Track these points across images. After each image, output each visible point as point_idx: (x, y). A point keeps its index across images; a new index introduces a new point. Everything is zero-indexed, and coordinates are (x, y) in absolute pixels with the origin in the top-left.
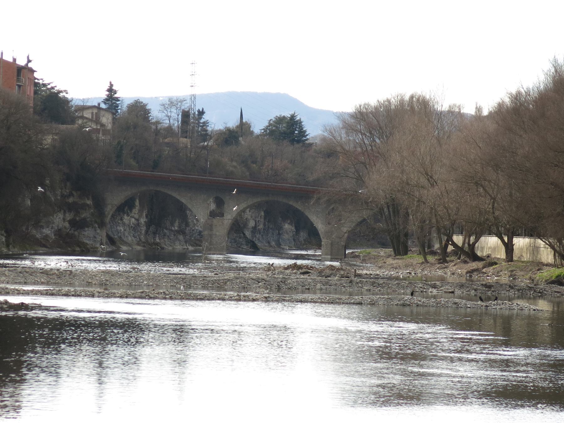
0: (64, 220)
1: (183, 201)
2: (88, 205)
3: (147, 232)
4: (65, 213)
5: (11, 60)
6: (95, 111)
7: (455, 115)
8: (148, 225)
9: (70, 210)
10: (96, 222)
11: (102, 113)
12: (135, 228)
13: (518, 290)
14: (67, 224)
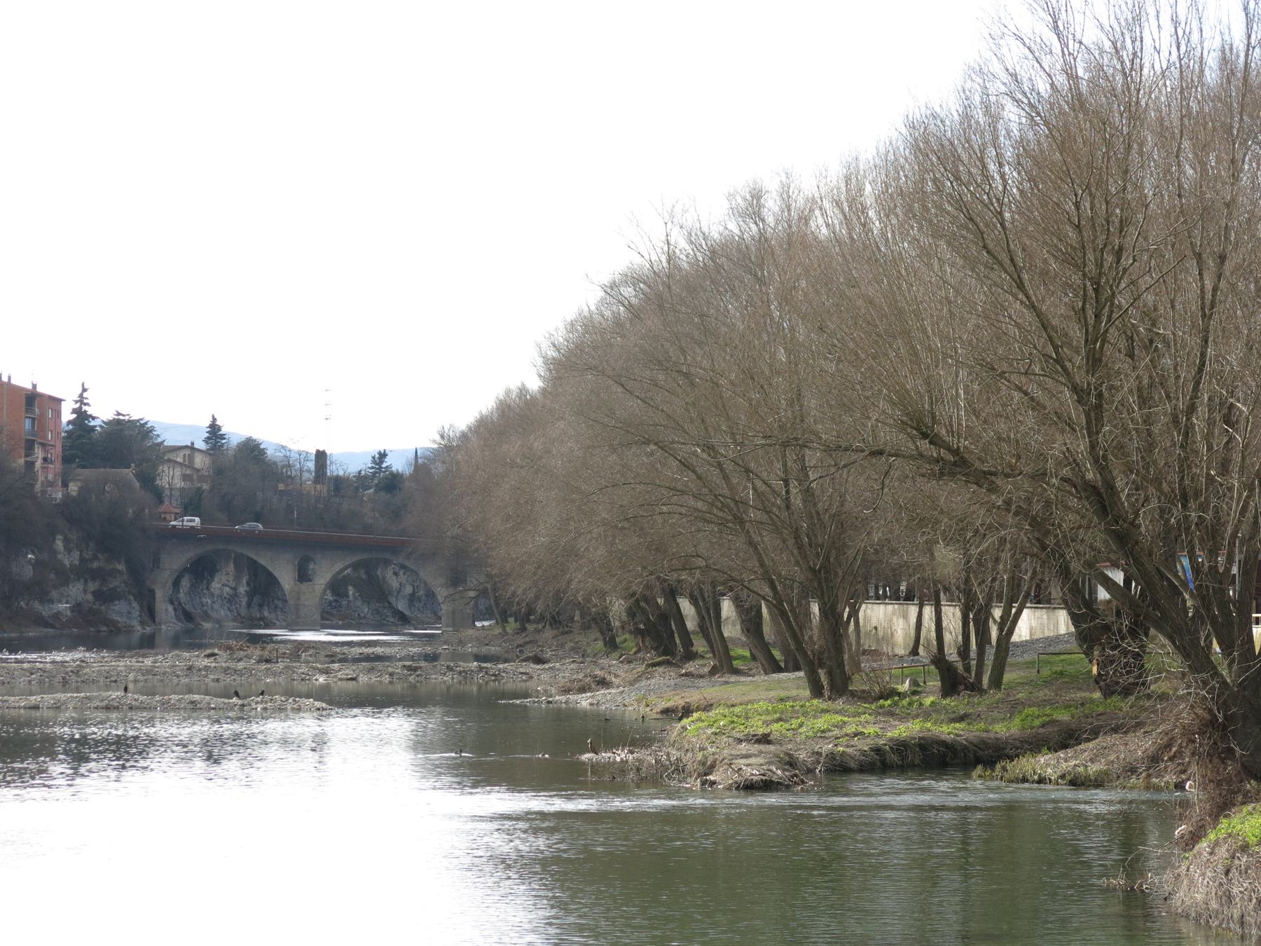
0: (85, 591)
1: (262, 562)
2: (119, 571)
3: (249, 605)
4: (86, 582)
5: (30, 387)
6: (187, 452)
7: (512, 421)
8: (251, 595)
9: (94, 579)
10: (130, 592)
11: (197, 454)
12: (232, 599)
13: (460, 673)
14: (90, 597)
